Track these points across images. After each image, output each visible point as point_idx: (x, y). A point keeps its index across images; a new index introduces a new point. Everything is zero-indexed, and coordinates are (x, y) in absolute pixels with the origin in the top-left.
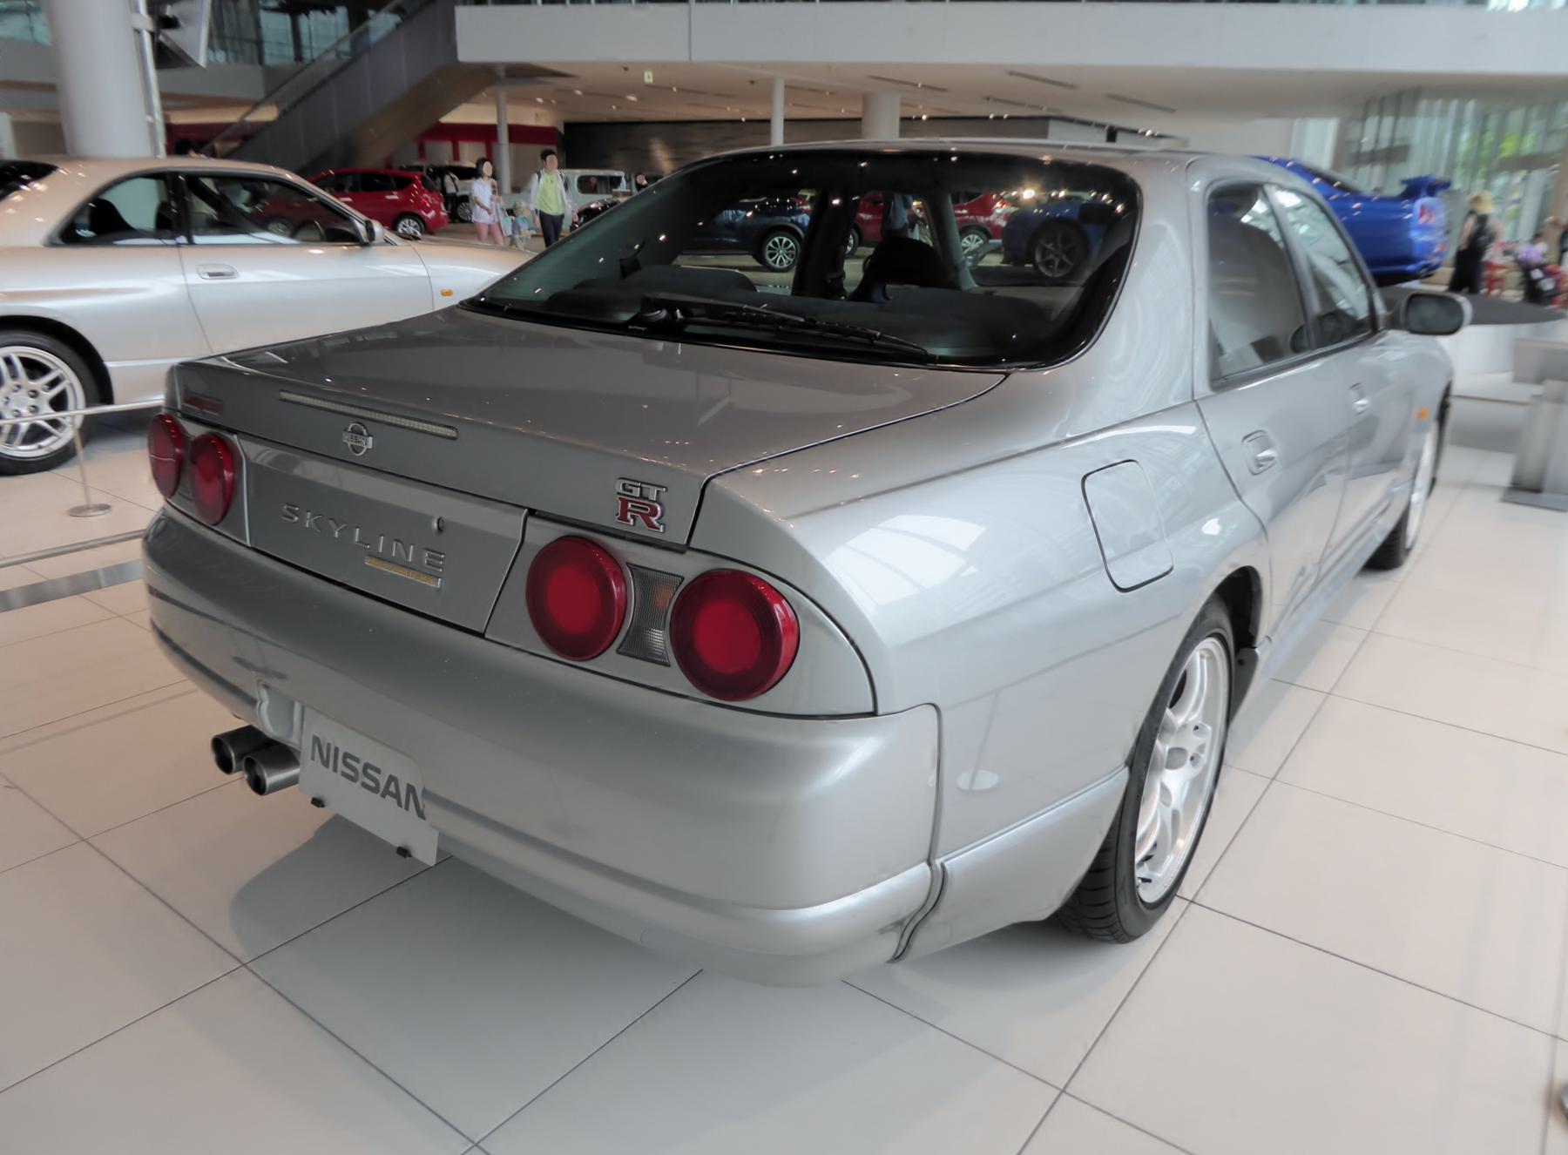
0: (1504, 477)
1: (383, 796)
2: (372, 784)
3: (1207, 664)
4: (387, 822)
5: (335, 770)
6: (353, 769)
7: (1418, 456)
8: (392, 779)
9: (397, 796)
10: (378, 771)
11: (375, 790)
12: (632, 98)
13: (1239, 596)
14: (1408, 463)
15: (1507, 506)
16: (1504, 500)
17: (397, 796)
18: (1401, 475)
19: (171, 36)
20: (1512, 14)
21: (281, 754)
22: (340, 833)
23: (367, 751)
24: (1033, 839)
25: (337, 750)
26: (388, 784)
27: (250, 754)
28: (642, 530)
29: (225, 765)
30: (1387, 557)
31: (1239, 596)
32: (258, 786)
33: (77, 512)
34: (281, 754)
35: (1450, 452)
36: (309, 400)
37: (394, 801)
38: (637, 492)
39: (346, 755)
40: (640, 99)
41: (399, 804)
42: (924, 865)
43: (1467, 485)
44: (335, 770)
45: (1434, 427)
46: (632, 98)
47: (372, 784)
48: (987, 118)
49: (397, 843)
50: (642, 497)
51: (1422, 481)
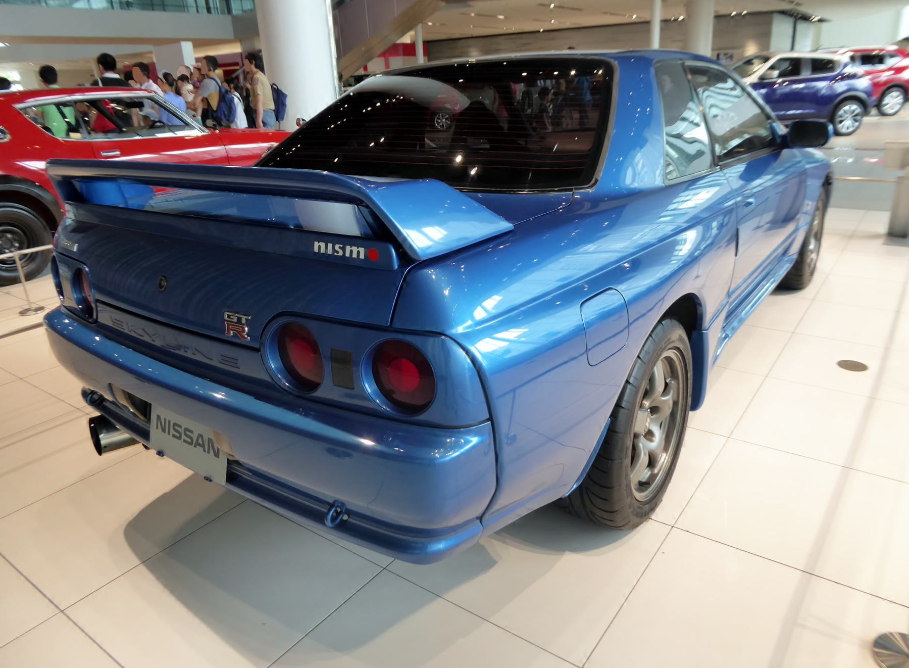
0: (883, 228)
1: (195, 446)
2: (178, 435)
5: (169, 433)
6: (186, 435)
10: (192, 432)
11: (191, 444)
15: (886, 247)
16: (885, 244)
17: (203, 446)
26: (197, 440)
30: (792, 283)
33: (23, 313)
36: (681, 386)
39: (175, 424)
41: (204, 451)
43: (852, 236)
44: (169, 433)
46: (501, 17)
47: (178, 435)
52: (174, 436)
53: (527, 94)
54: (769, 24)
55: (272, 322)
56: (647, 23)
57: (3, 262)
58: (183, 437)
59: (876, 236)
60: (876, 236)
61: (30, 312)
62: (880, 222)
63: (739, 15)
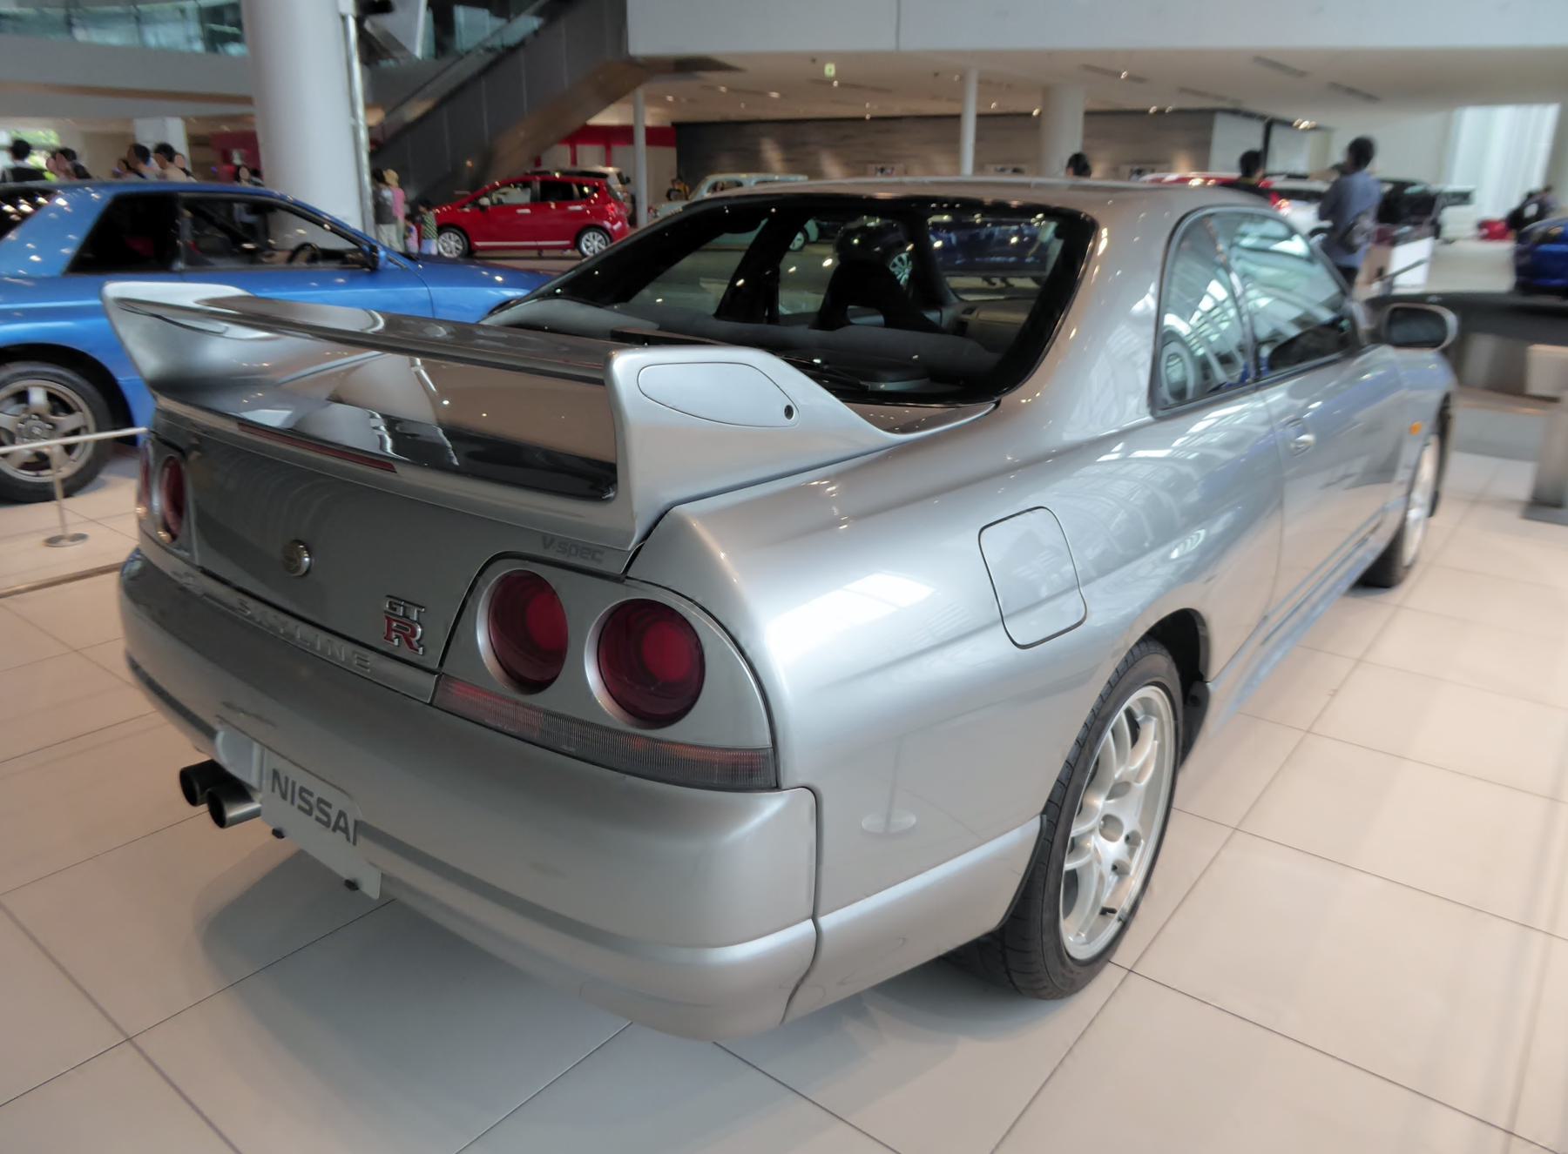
1: (334, 830)
3: (1151, 699)
4: (342, 857)
6: (322, 811)
7: (1416, 468)
8: (341, 814)
9: (345, 830)
10: (329, 806)
11: (327, 824)
12: (775, 95)
13: (1180, 641)
14: (1402, 475)
17: (345, 830)
18: (1395, 493)
19: (378, 24)
20: (781, 258)
21: (241, 792)
22: (301, 865)
23: (319, 790)
24: (962, 875)
25: (294, 784)
27: (211, 788)
28: (405, 652)
29: (192, 799)
31: (1180, 641)
32: (220, 820)
33: (52, 542)
34: (241, 792)
35: (1456, 459)
37: (343, 835)
38: (400, 611)
39: (302, 790)
40: (783, 96)
42: (810, 923)
45: (1434, 440)
46: (775, 95)
48: (1145, 112)
49: (346, 877)
50: (405, 616)
51: (1421, 496)
52: (300, 808)
53: (1267, 286)
54: (1209, 128)
55: (491, 568)
56: (957, 118)
57: (5, 456)
58: (316, 813)
59: (1505, 503)
60: (1505, 503)
61: (63, 542)
62: (1519, 481)
63: (1160, 112)
